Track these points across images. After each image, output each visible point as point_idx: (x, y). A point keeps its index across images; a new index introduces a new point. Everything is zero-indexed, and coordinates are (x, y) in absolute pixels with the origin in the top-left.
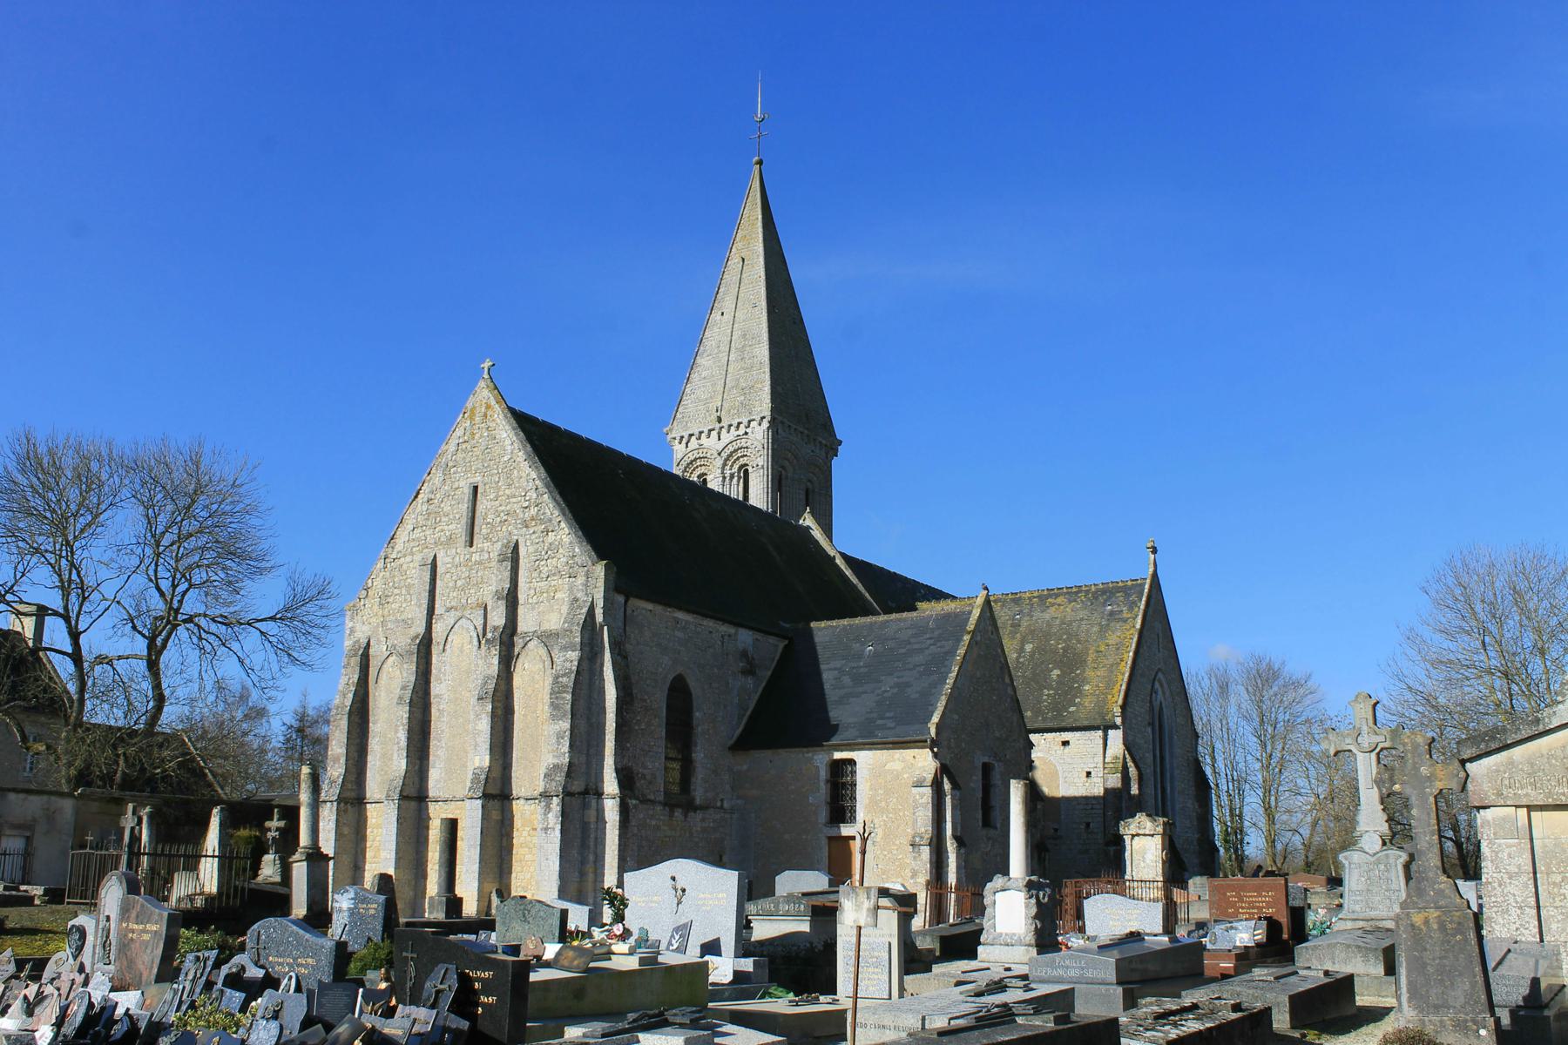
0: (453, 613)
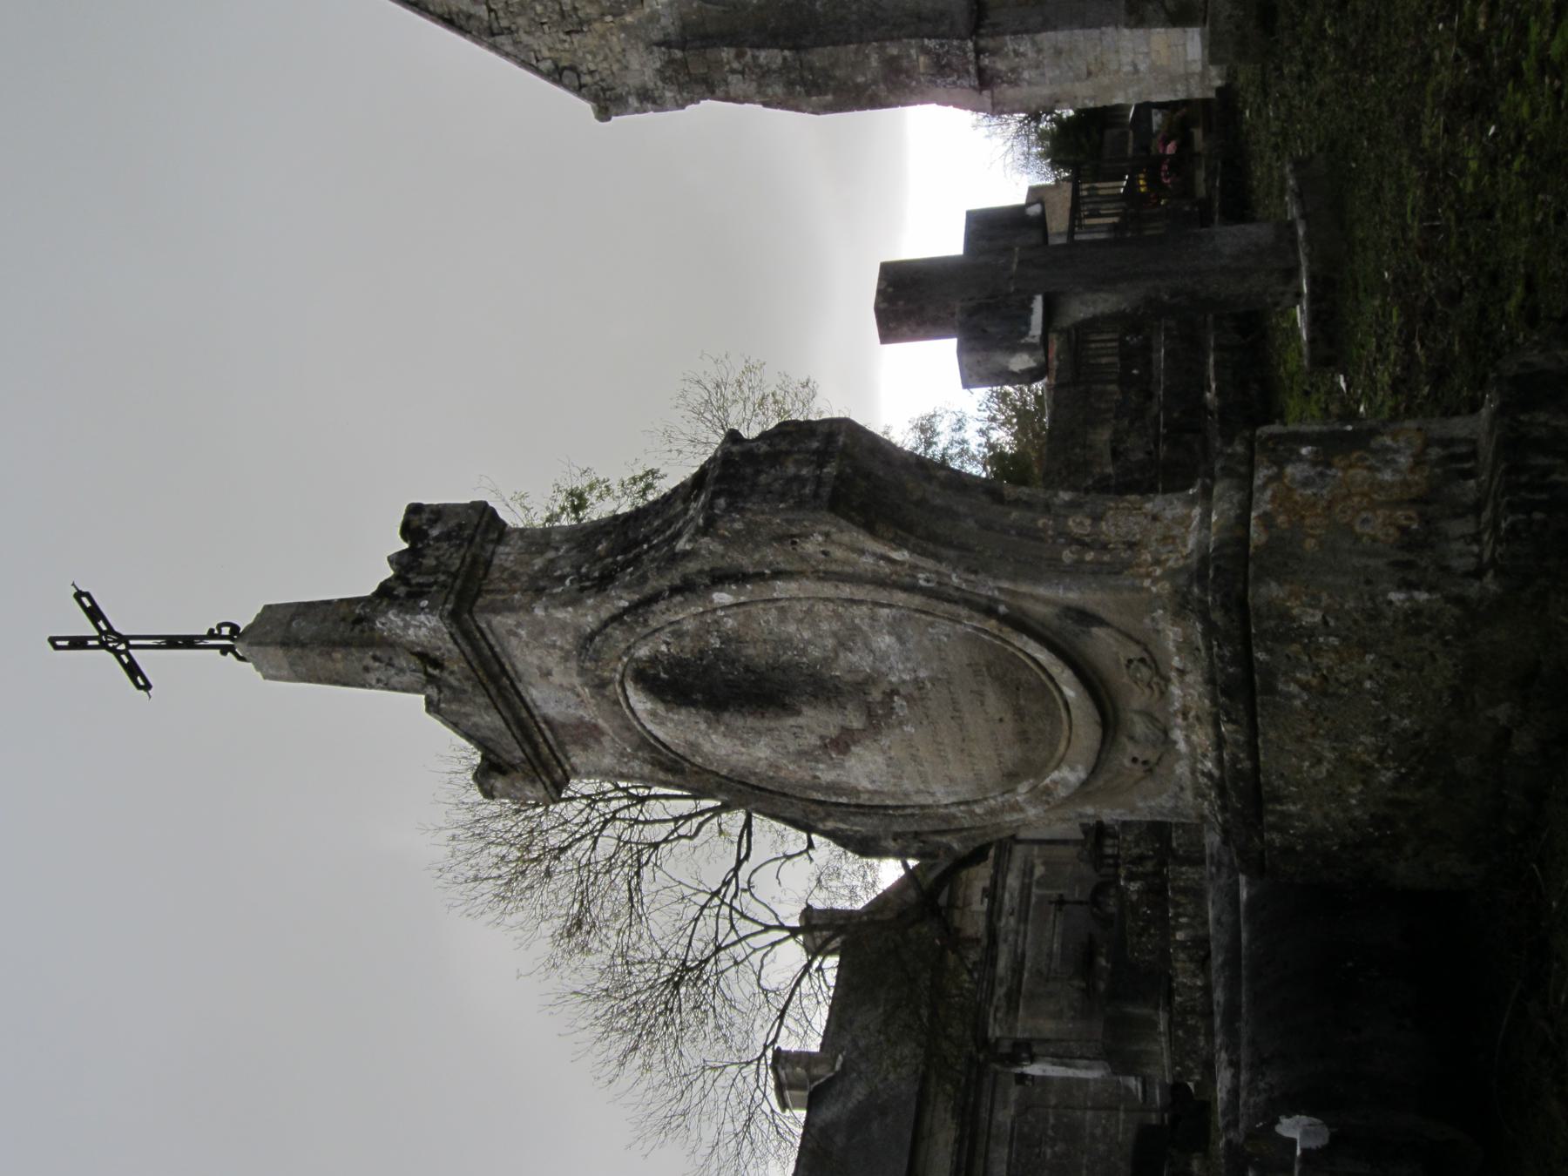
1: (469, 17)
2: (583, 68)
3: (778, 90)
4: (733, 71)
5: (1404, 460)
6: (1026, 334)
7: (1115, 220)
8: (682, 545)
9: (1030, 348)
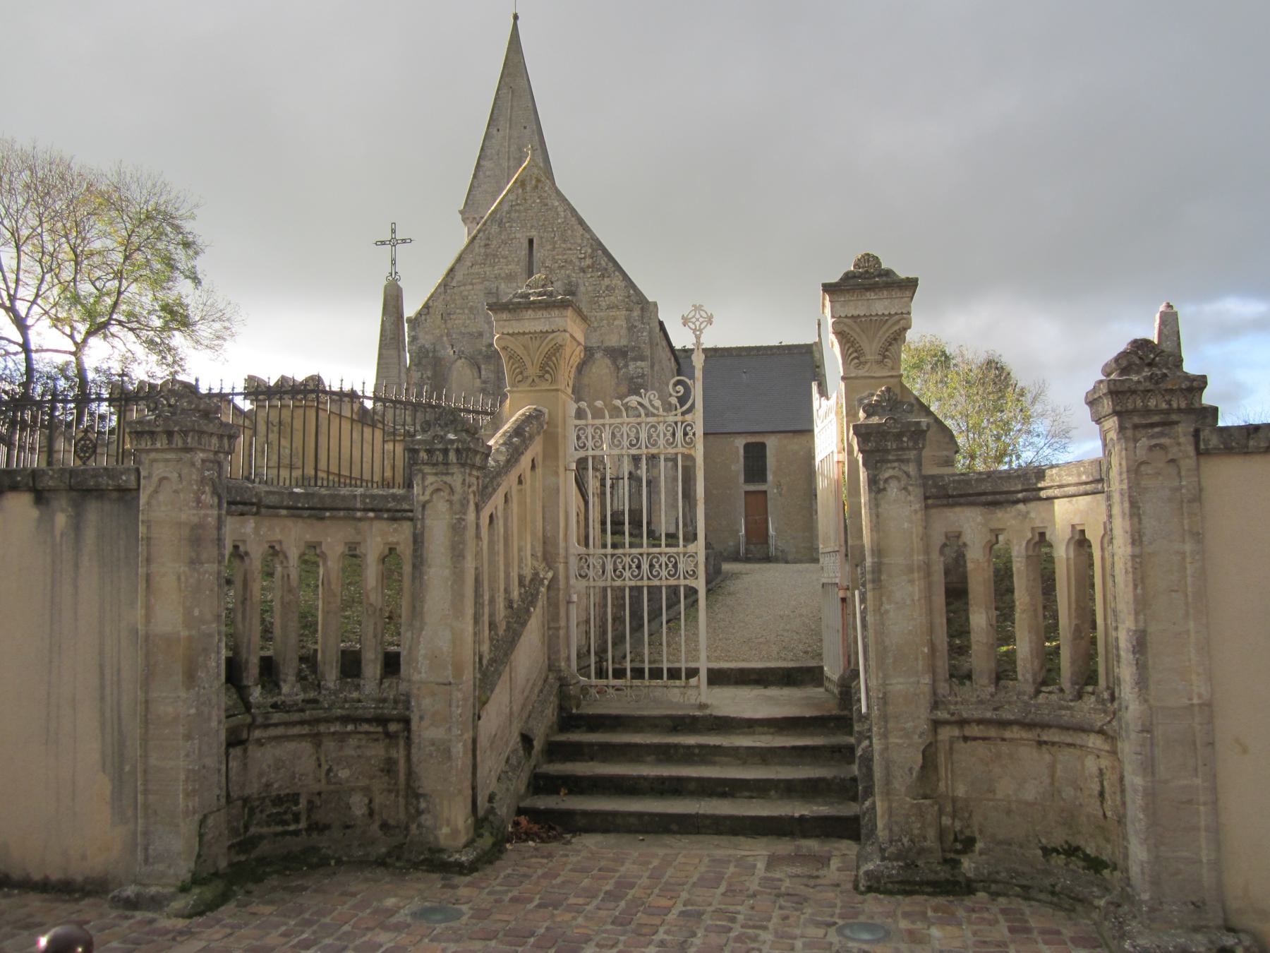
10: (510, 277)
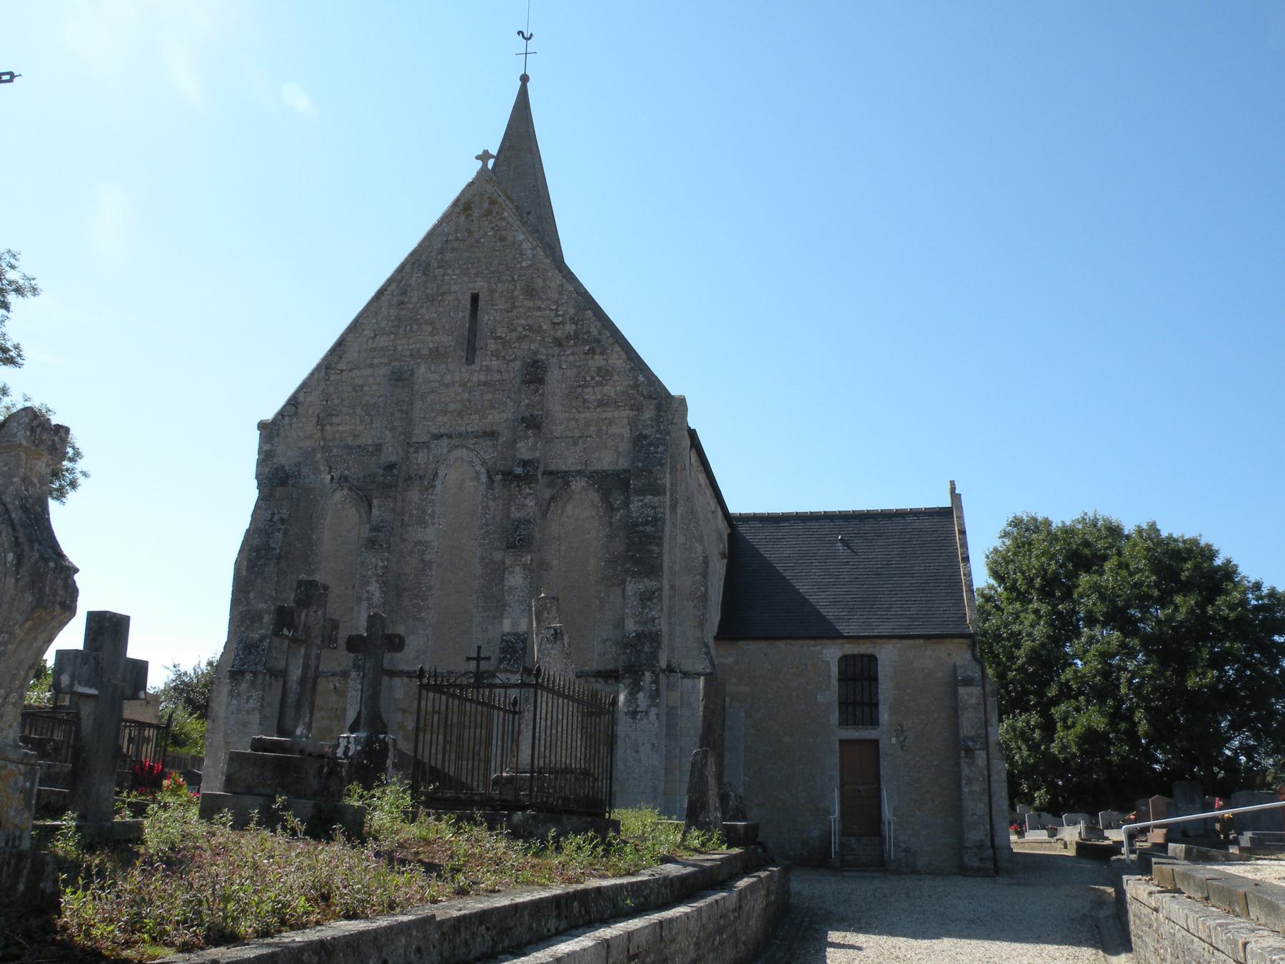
0: (445, 441)
1: (340, 357)
2: (294, 420)
3: (256, 542)
4: (273, 514)
5: (17, 821)
6: (80, 683)
7: (125, 750)
8: (36, 546)
9: (72, 685)
10: (437, 355)
